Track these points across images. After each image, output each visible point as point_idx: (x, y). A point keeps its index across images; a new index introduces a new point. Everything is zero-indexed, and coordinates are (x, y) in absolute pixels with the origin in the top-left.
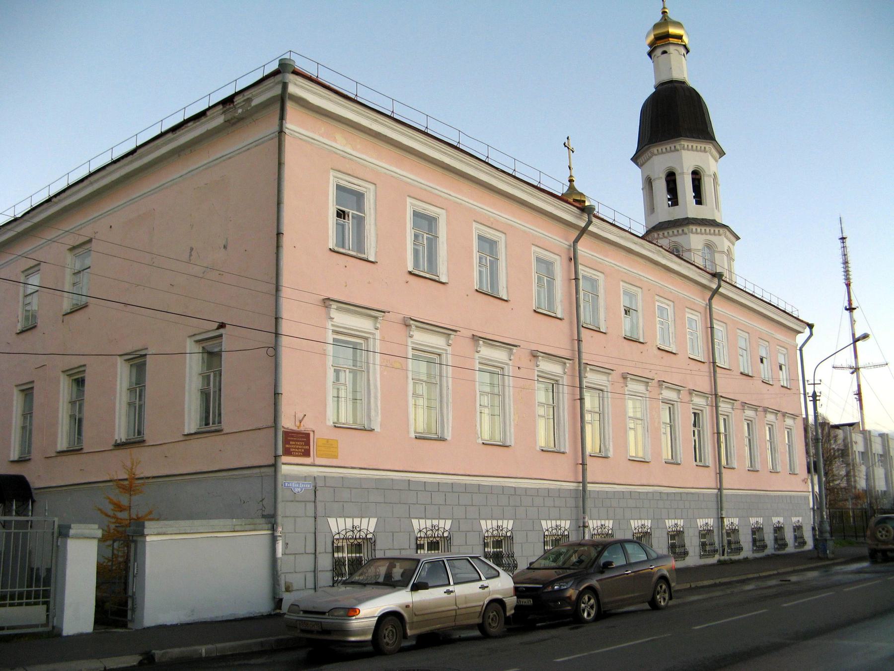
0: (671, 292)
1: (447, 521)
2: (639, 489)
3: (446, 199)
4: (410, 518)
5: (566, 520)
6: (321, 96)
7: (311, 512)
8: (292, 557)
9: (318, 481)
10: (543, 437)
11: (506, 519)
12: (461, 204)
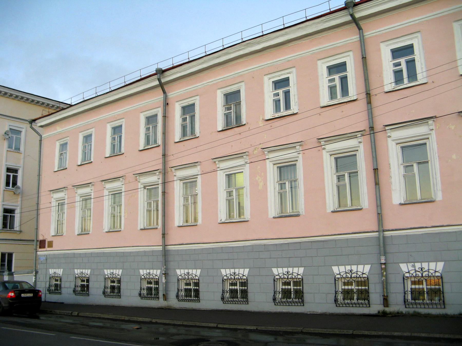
0: (289, 61)
1: (197, 270)
2: (230, 244)
3: (94, 122)
4: (74, 269)
5: (157, 269)
6: (44, 121)
7: (45, 267)
8: (40, 282)
9: (47, 256)
10: (142, 222)
11: (118, 269)
12: (100, 120)
